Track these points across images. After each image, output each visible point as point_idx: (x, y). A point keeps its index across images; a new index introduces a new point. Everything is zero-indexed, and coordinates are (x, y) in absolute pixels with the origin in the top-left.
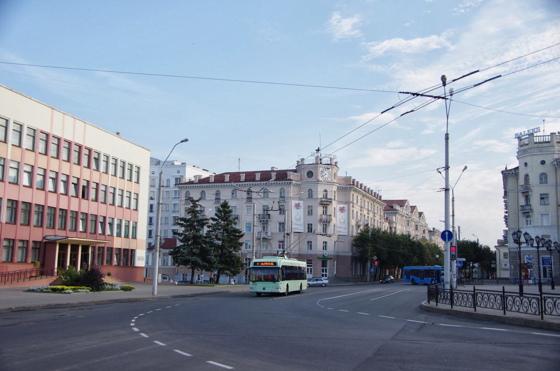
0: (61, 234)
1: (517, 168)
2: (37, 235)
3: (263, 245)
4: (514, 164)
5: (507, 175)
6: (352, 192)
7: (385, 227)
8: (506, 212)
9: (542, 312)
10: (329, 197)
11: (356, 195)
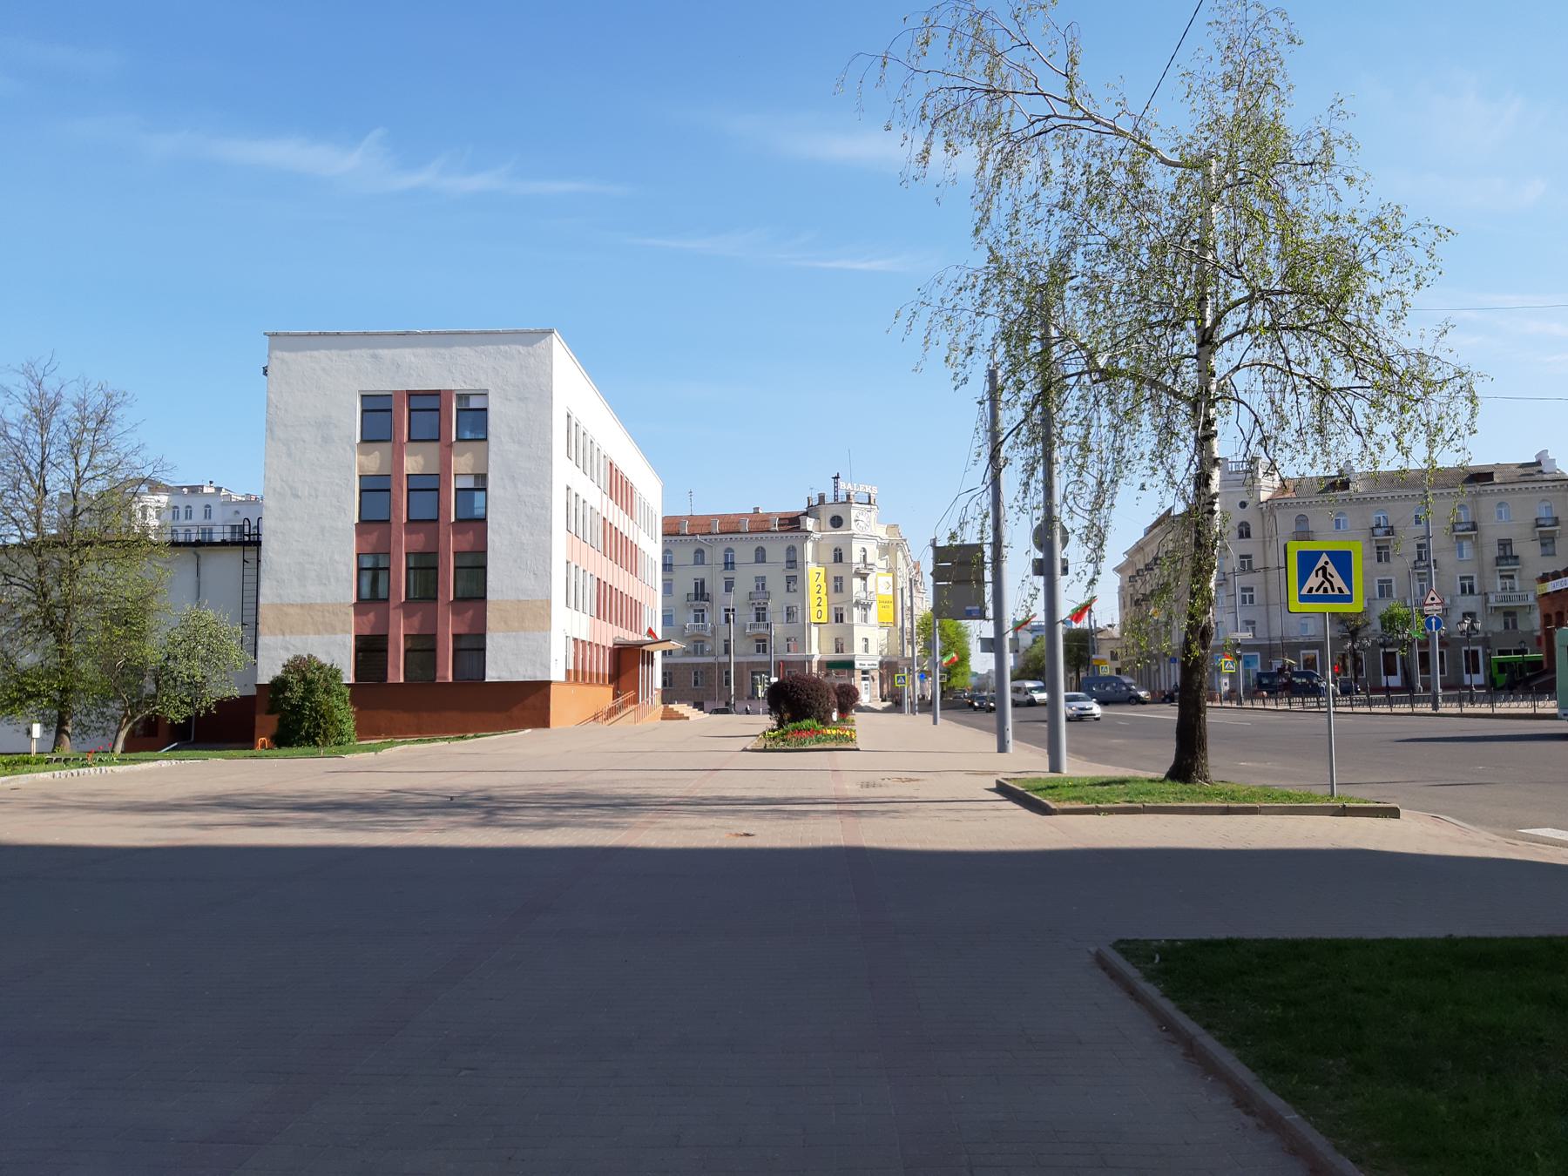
10: (869, 561)
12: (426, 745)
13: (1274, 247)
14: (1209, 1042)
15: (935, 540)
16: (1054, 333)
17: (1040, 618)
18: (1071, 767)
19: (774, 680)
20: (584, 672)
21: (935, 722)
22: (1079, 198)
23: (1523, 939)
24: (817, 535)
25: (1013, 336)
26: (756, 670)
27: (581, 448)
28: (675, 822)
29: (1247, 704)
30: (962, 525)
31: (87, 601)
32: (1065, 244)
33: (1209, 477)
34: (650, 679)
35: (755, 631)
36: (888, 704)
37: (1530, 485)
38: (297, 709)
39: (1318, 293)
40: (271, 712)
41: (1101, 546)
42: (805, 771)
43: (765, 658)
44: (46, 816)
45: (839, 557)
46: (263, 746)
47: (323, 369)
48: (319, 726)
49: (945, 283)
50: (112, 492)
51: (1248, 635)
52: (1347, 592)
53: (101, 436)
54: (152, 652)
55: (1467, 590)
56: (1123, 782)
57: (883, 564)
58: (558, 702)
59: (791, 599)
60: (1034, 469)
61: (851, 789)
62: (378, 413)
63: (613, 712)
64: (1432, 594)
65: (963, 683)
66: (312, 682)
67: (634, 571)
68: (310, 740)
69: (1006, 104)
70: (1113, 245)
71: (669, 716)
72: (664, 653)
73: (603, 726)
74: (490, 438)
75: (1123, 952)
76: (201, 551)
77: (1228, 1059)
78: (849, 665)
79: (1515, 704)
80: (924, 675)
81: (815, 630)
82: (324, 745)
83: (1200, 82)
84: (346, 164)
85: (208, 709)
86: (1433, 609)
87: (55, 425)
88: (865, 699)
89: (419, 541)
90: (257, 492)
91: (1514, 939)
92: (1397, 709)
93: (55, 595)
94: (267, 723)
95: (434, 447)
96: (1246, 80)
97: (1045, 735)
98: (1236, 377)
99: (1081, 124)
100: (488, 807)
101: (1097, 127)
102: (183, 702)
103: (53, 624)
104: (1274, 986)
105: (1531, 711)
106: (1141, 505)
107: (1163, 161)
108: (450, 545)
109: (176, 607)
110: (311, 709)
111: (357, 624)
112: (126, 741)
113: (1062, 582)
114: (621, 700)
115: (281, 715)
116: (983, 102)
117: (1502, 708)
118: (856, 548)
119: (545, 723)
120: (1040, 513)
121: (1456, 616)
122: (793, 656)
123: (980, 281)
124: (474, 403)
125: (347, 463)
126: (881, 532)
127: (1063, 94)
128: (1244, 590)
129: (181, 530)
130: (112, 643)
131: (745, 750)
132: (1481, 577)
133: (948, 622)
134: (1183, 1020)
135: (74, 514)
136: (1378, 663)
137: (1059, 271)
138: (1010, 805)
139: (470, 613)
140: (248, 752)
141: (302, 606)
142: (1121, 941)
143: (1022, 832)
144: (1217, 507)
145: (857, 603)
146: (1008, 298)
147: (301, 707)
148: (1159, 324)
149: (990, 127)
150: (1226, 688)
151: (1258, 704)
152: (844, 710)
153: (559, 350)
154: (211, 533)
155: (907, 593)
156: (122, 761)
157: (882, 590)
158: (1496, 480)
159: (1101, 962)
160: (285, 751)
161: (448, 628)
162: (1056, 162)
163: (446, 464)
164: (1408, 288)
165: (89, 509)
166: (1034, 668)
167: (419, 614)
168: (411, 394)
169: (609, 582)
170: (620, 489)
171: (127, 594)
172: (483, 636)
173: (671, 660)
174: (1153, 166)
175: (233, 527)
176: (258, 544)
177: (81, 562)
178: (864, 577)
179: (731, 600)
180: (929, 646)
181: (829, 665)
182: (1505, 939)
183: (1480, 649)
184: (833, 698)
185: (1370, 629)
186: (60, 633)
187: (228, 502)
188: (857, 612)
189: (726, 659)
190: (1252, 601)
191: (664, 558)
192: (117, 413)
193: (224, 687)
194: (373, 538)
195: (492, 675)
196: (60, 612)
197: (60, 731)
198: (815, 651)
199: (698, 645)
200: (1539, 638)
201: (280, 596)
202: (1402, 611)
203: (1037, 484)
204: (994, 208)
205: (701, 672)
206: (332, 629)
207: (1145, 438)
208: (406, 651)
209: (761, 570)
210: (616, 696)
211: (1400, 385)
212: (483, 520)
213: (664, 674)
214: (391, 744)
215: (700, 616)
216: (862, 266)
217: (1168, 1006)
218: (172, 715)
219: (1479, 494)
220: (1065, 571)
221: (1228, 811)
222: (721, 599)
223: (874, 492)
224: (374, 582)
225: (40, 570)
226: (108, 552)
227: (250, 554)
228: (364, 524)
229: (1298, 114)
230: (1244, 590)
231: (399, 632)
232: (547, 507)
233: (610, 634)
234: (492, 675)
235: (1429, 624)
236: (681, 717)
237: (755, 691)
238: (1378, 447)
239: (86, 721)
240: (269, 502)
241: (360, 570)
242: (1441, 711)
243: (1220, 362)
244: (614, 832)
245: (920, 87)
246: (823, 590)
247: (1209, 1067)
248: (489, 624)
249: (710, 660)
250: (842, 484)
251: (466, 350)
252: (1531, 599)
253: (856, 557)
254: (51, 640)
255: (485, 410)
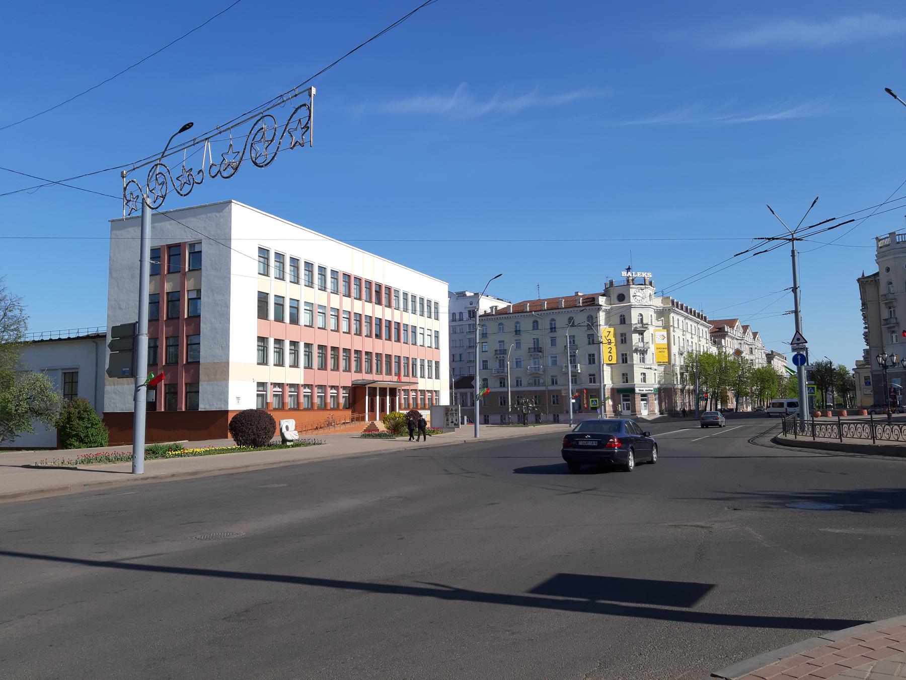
0: (369, 377)
1: (877, 274)
2: (347, 379)
3: (503, 383)
4: (872, 268)
5: (865, 283)
6: (672, 315)
7: (714, 350)
8: (866, 328)
9: (841, 436)
10: (645, 322)
11: (676, 317)
57: (660, 323)
78: (632, 390)
126: (658, 302)
163: (183, 285)
178: (641, 333)
195: (202, 407)
234: (202, 407)
249: (543, 388)
253: (635, 319)
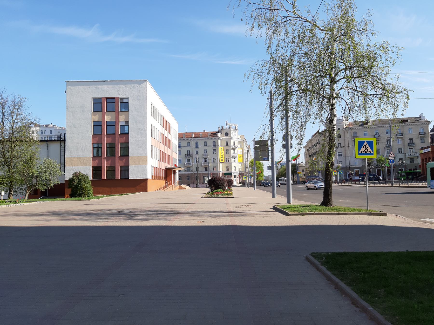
10: (236, 145)
12: (113, 197)
13: (352, 55)
14: (342, 284)
15: (254, 139)
16: (289, 79)
17: (284, 160)
18: (293, 202)
19: (210, 178)
20: (157, 176)
21: (254, 190)
22: (296, 40)
23: (429, 252)
24: (221, 138)
25: (277, 80)
26: (205, 175)
27: (155, 113)
28: (183, 218)
29: (340, 184)
30: (264, 134)
31: (16, 157)
32: (292, 54)
33: (333, 120)
34: (175, 178)
35: (204, 165)
36: (240, 185)
37: (418, 123)
38: (76, 187)
39: (364, 67)
40: (69, 188)
41: (302, 140)
42: (219, 204)
43: (207, 172)
44: (3, 218)
45: (227, 144)
46: (67, 197)
47: (82, 91)
48: (82, 192)
49: (258, 65)
50: (23, 126)
51: (340, 165)
52: (372, 152)
53: (19, 110)
54: (35, 171)
55: (400, 152)
56: (309, 206)
57: (239, 146)
58: (150, 184)
59: (214, 156)
60: (283, 118)
61: (232, 208)
62: (98, 104)
63: (165, 187)
64: (391, 153)
65: (262, 179)
66: (80, 179)
67: (170, 148)
68: (80, 195)
69: (275, 14)
70: (306, 54)
71: (181, 188)
72: (179, 171)
73: (162, 191)
74: (129, 111)
75: (314, 256)
76: (48, 143)
77: (348, 290)
78: (230, 174)
79: (414, 184)
80: (251, 176)
81: (221, 164)
82: (84, 196)
83: (330, 6)
84: (88, 34)
85: (51, 187)
86: (392, 158)
87: (6, 107)
88: (235, 183)
89: (110, 140)
90: (64, 126)
91: (427, 252)
92: (382, 185)
93: (7, 155)
94: (68, 191)
95: (114, 113)
96: (344, 6)
97: (286, 193)
98: (341, 91)
99: (297, 19)
100: (129, 214)
101: (301, 20)
102: (44, 185)
103: (7, 164)
104: (362, 267)
105: (419, 185)
106: (314, 126)
107: (320, 29)
108: (119, 141)
109: (42, 158)
110: (80, 187)
111: (93, 163)
112: (29, 196)
113: (291, 150)
114: (167, 184)
115: (72, 189)
116: (269, 13)
117: (411, 185)
118: (232, 141)
119: (146, 191)
120: (285, 131)
121: (397, 160)
122: (215, 172)
123: (268, 64)
124: (125, 101)
125: (89, 118)
126: (239, 137)
127: (292, 10)
128: (339, 152)
129: (43, 137)
130: (24, 169)
131: (202, 198)
132: (404, 149)
133: (258, 162)
134: (334, 277)
135: (13, 133)
136: (376, 173)
137: (291, 60)
138: (277, 213)
139: (125, 160)
140: (63, 199)
141: (77, 158)
142: (313, 253)
143: (280, 221)
144: (335, 129)
145: (233, 157)
146: (276, 69)
147: (77, 186)
148: (319, 76)
149: (271, 20)
150: (334, 180)
151: (343, 184)
152: (229, 187)
153: (149, 88)
154: (52, 138)
155: (246, 154)
156: (27, 202)
157: (239, 153)
158: (408, 122)
159: (307, 259)
160: (73, 199)
161: (119, 164)
162: (290, 29)
163: (117, 118)
164: (391, 65)
165: (16, 131)
166: (282, 174)
167: (110, 161)
168: (107, 98)
169: (164, 151)
170: (166, 125)
171: (27, 155)
172: (128, 166)
173: (181, 173)
174: (317, 31)
175: (58, 136)
176: (65, 141)
177: (15, 146)
178: (234, 150)
179: (198, 156)
180: (253, 169)
181: (225, 174)
182: (423, 252)
183: (404, 168)
184: (226, 183)
185: (373, 163)
186: (9, 166)
187: (56, 129)
188: (232, 159)
189: (196, 172)
190: (341, 156)
191: (179, 144)
192: (24, 104)
193: (56, 181)
194: (97, 139)
195: (131, 177)
196: (9, 160)
197: (10, 194)
198: (221, 170)
199: (188, 169)
200: (420, 166)
201: (71, 155)
202: (382, 158)
203: (284, 123)
204: (272, 43)
205: (189, 176)
206: (86, 165)
207: (314, 109)
208: (107, 171)
209: (206, 148)
210: (166, 183)
211: (387, 93)
212: (128, 134)
213: (179, 177)
214: (103, 197)
215: (189, 160)
216: (233, 63)
217: (329, 273)
218: (41, 189)
219: (404, 126)
220: (292, 147)
221: (338, 214)
222: (195, 156)
223: (237, 126)
224: (98, 151)
225: (3, 148)
226: (22, 143)
227: (62, 144)
228: (94, 135)
229: (358, 16)
230: (339, 152)
231: (105, 165)
232: (146, 130)
233: (164, 166)
234: (131, 177)
235: (391, 162)
236: (184, 189)
237: (204, 181)
238: (379, 112)
239: (17, 190)
240: (67, 129)
241: (93, 148)
242: (394, 185)
243: (337, 87)
244: (166, 221)
245: (251, 8)
246: (223, 153)
247: (343, 292)
248: (130, 163)
250: (228, 124)
251: (122, 86)
252: (418, 154)
253: (232, 144)
254: (6, 168)
255: (128, 103)
